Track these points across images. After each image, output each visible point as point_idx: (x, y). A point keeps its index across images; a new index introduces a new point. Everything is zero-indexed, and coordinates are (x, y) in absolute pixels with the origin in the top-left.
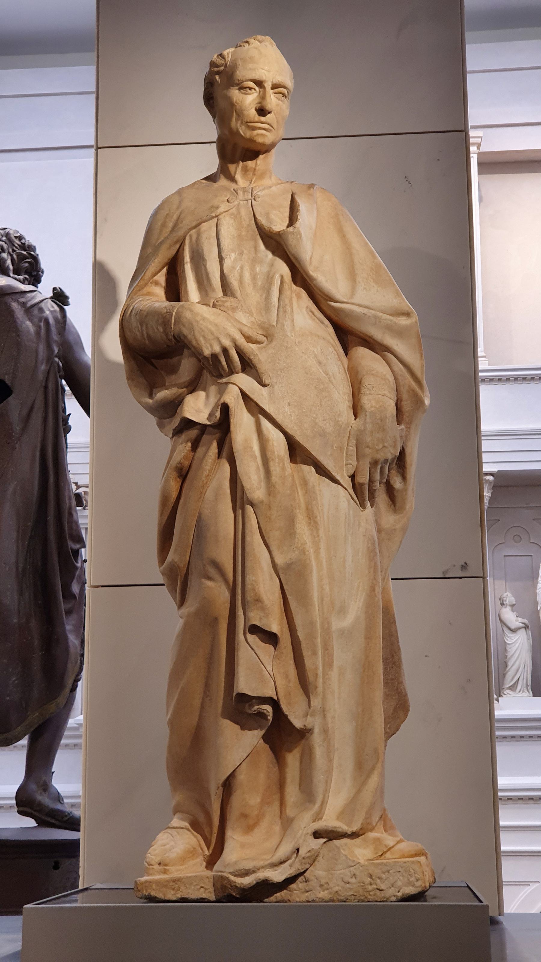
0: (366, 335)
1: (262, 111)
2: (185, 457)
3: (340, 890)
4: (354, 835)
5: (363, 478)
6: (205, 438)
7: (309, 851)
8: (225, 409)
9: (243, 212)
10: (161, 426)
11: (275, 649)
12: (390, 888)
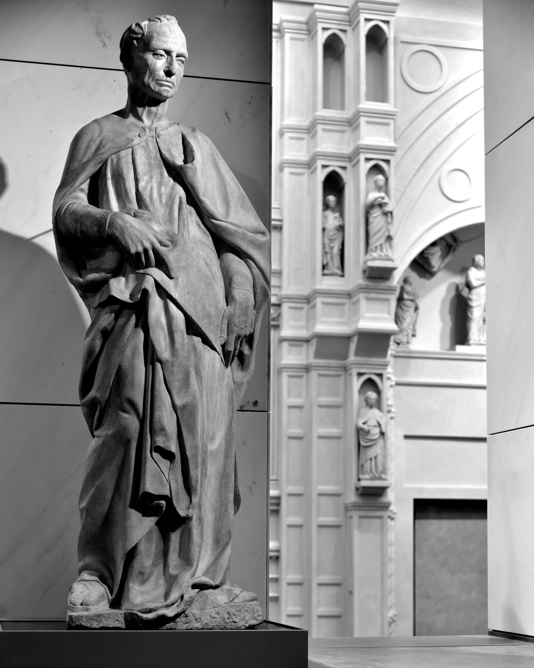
1: (169, 73)
2: (109, 324)
4: (216, 587)
5: (231, 348)
7: (190, 597)
8: (145, 293)
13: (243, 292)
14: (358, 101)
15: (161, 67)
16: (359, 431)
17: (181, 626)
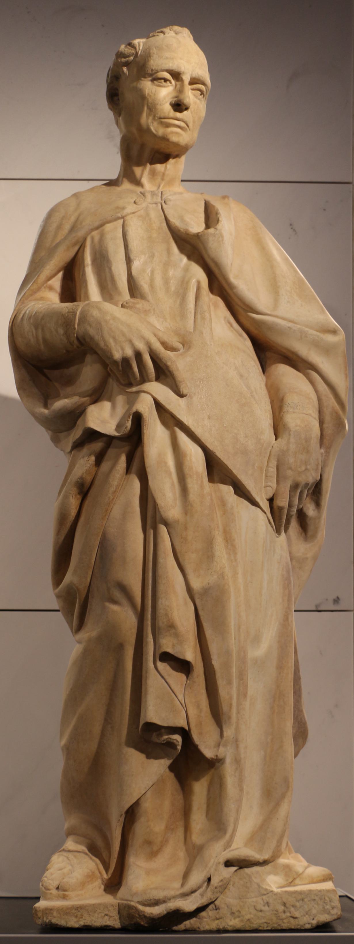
0: (289, 350)
1: (179, 106)
3: (253, 918)
4: (265, 863)
5: (283, 502)
6: (111, 452)
7: (222, 881)
8: (138, 419)
10: (56, 440)
12: (305, 916)
17: (209, 925)
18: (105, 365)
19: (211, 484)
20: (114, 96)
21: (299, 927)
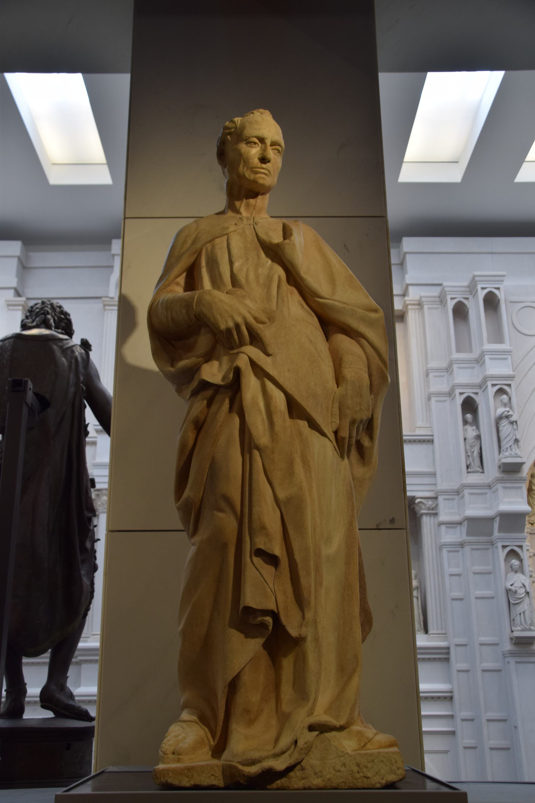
1: (264, 160)
4: (341, 728)
5: (345, 433)
6: (218, 397)
7: (306, 743)
8: (237, 372)
9: (248, 232)
10: (179, 391)
11: (276, 569)
13: (356, 368)
14: (482, 344)
15: (254, 155)
16: (508, 591)
18: (214, 334)
19: (291, 420)
20: (222, 155)
21: (371, 786)
